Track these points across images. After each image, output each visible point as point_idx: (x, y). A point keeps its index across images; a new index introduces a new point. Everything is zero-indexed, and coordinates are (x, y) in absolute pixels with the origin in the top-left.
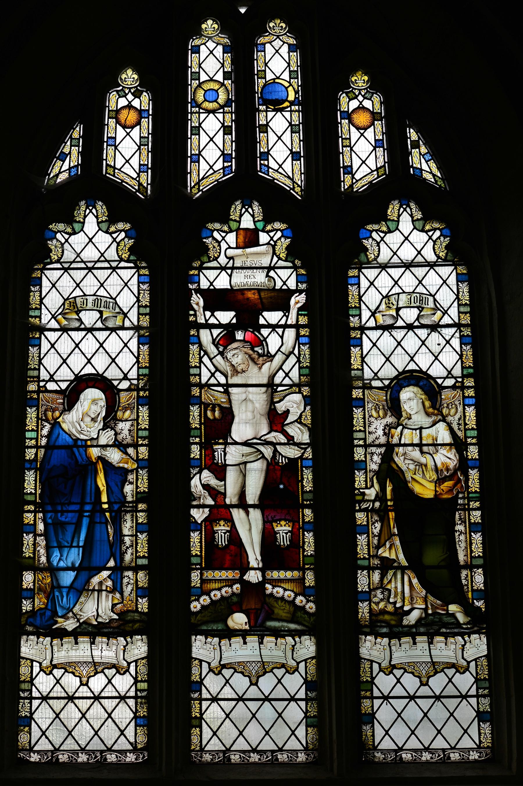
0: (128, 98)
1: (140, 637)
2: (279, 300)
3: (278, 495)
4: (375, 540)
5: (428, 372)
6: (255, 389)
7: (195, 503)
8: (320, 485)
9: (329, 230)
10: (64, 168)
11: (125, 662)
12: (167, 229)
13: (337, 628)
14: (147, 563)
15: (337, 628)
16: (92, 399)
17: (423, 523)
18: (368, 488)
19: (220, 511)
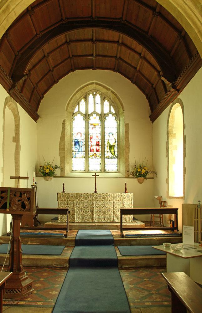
0: (83, 102)
1: (159, 215)
3: (97, 144)
4: (107, 149)
6: (95, 133)
7: (176, 86)
8: (101, 144)
9: (102, 117)
11: (39, 96)
12: (87, 117)
13: (103, 157)
15: (103, 157)
17: (111, 147)
18: (106, 144)
19: (91, 146)
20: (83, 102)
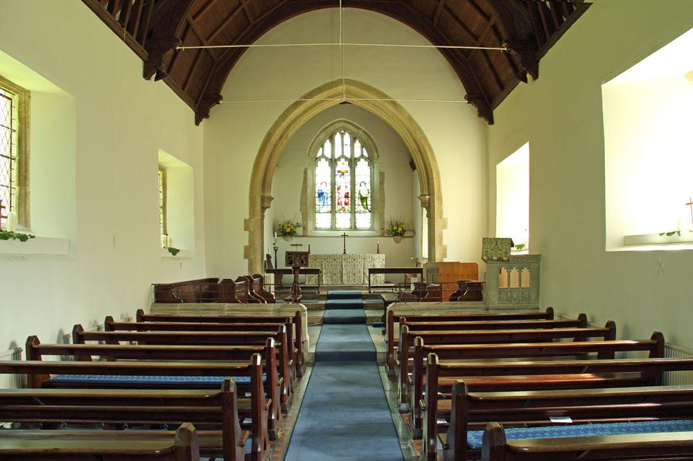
0: (328, 144)
2: (347, 172)
3: (346, 196)
4: (358, 202)
5: (278, 268)
6: (344, 182)
8: (351, 196)
9: (353, 162)
10: (320, 154)
12: (333, 162)
13: (353, 212)
14: (250, 381)
15: (353, 212)
16: (324, 184)
17: (363, 199)
18: (357, 195)
20: (328, 144)
